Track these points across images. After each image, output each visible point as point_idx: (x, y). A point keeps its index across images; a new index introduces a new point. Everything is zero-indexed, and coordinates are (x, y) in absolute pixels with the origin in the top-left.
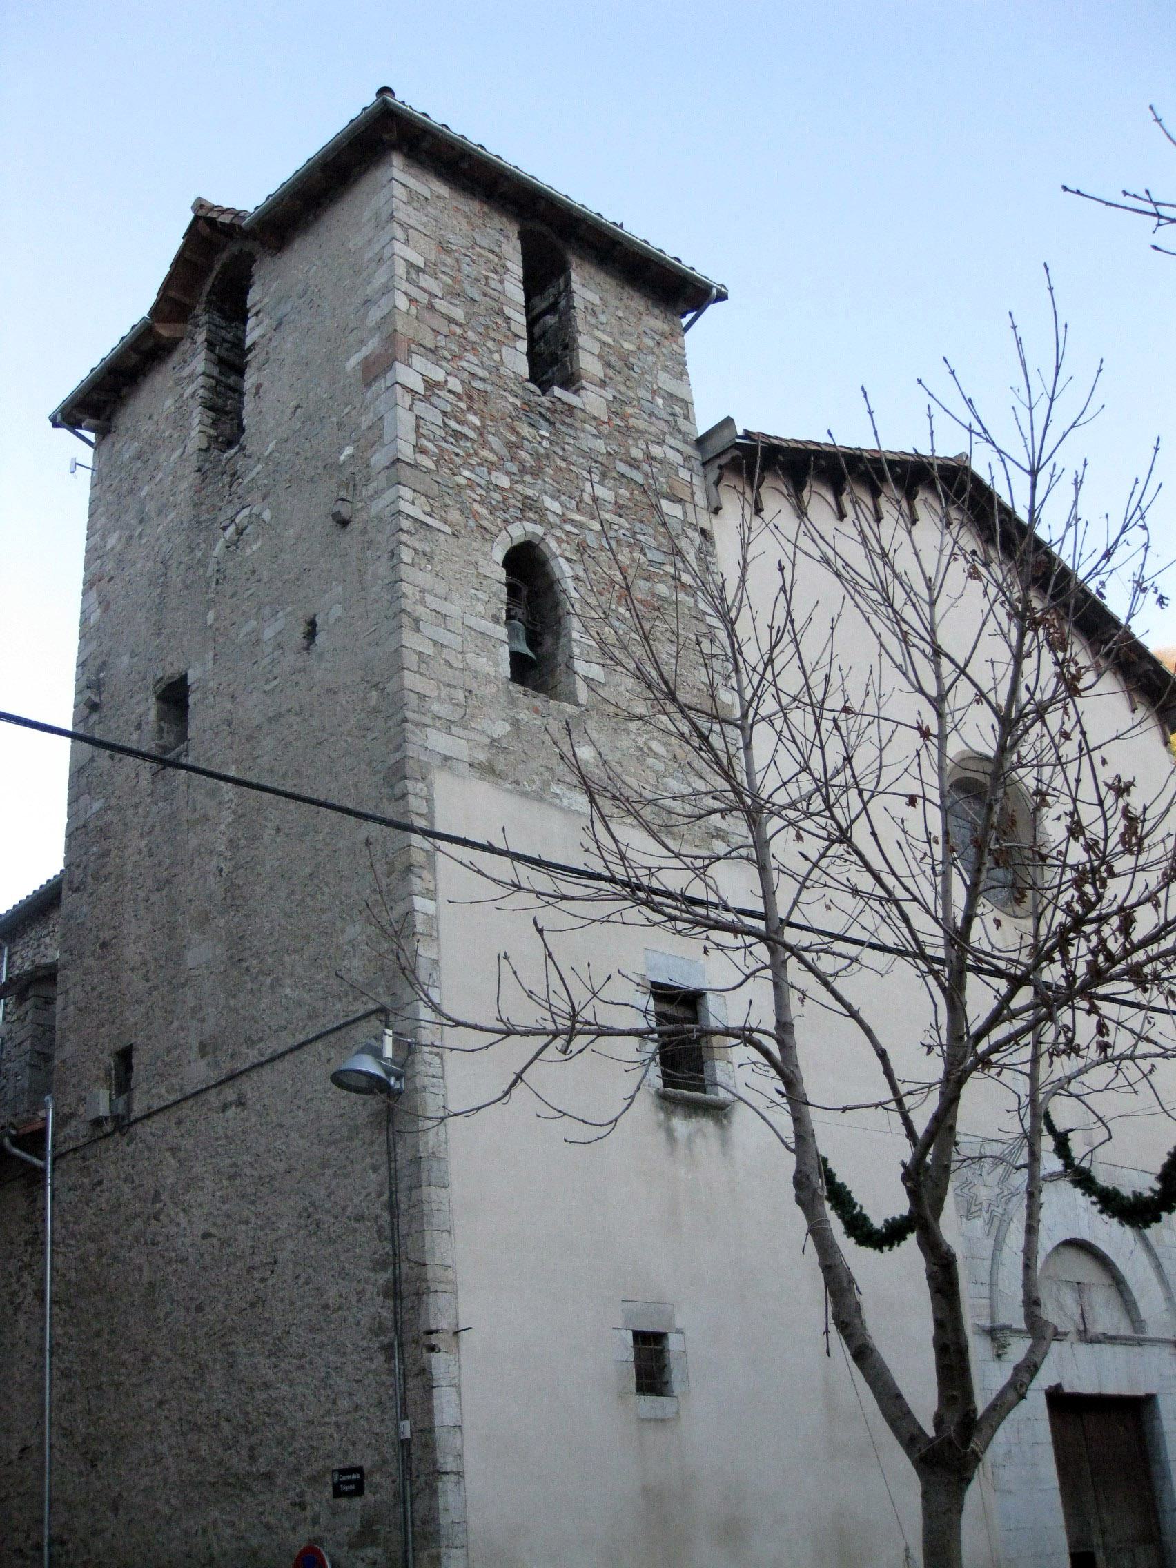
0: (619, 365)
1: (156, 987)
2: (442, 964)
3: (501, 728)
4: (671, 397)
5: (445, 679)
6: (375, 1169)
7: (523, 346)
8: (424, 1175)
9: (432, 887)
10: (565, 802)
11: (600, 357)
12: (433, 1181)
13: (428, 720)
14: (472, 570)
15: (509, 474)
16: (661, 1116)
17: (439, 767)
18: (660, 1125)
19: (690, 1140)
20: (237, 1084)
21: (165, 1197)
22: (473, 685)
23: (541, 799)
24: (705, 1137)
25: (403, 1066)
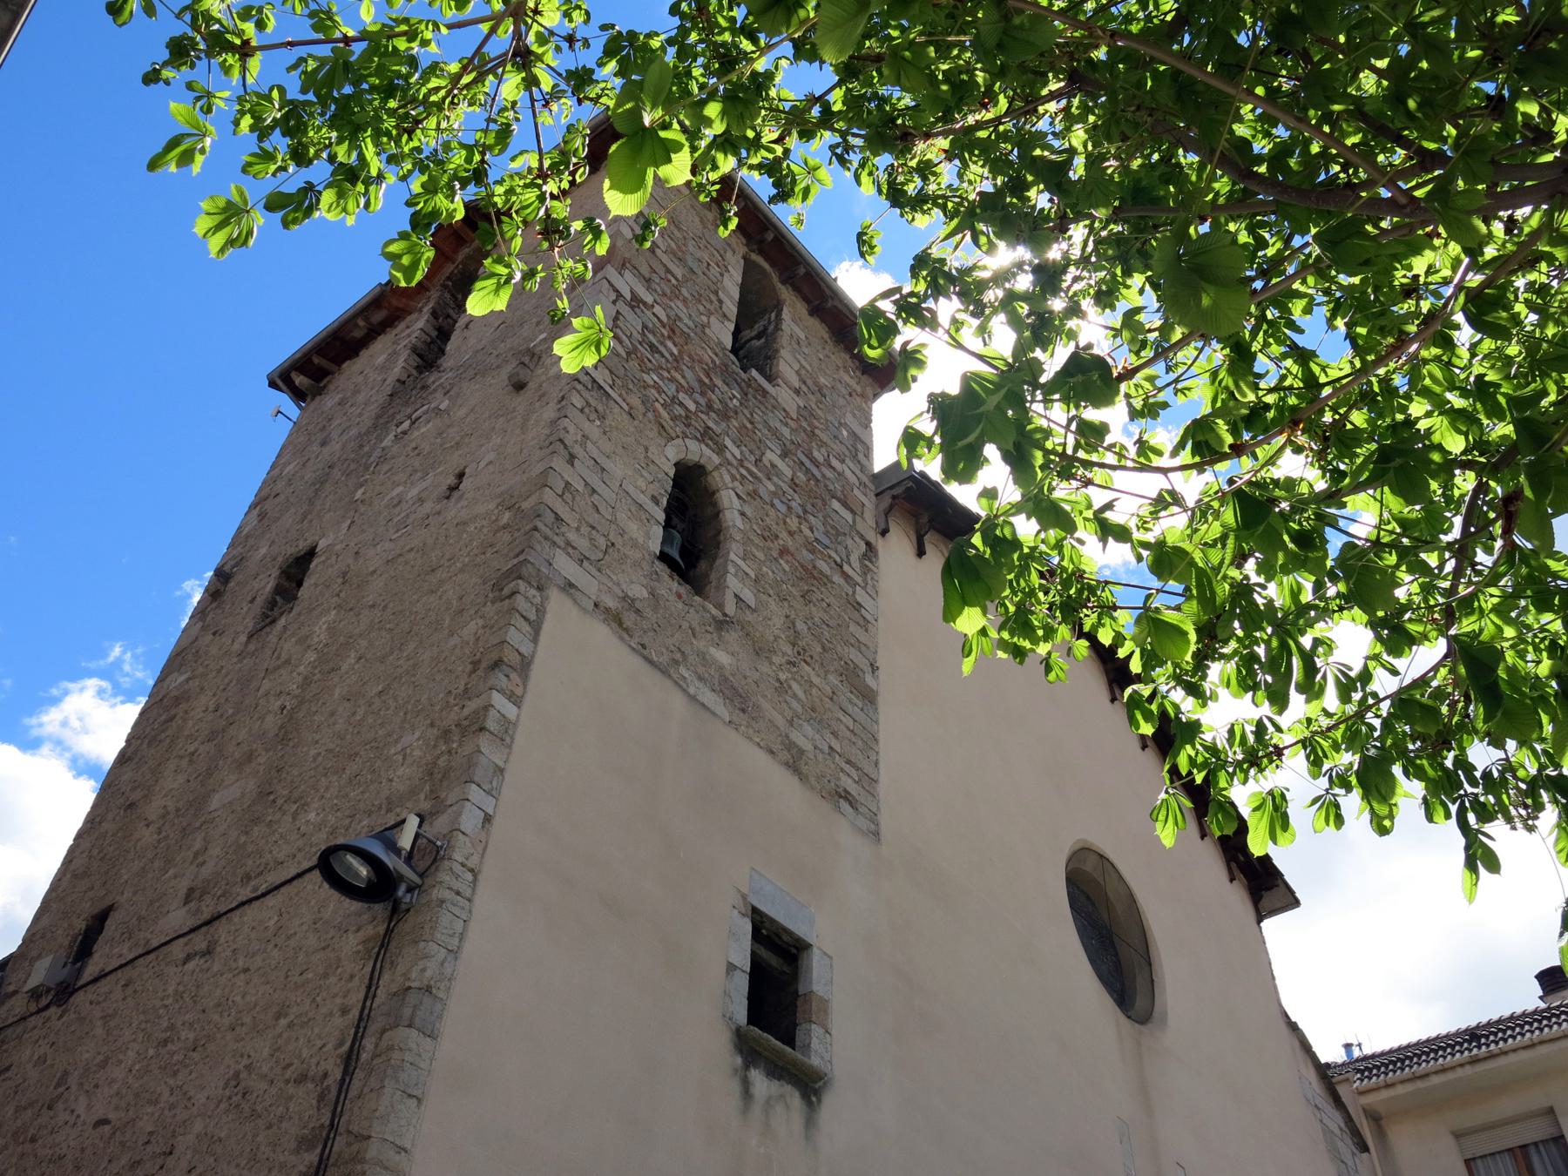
0: (808, 386)
1: (166, 838)
2: (507, 775)
3: (639, 592)
4: (853, 434)
5: (591, 521)
6: (344, 1011)
7: (732, 327)
8: (407, 1012)
9: (519, 692)
10: (692, 690)
11: (797, 372)
12: (417, 1021)
13: (559, 541)
14: (641, 450)
15: (696, 403)
16: (739, 1060)
17: (559, 586)
18: (736, 1070)
19: (768, 1104)
20: (212, 930)
21: (73, 1081)
22: (619, 542)
23: (665, 673)
24: (787, 1107)
25: (421, 876)
